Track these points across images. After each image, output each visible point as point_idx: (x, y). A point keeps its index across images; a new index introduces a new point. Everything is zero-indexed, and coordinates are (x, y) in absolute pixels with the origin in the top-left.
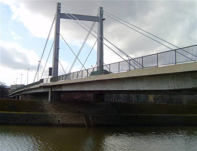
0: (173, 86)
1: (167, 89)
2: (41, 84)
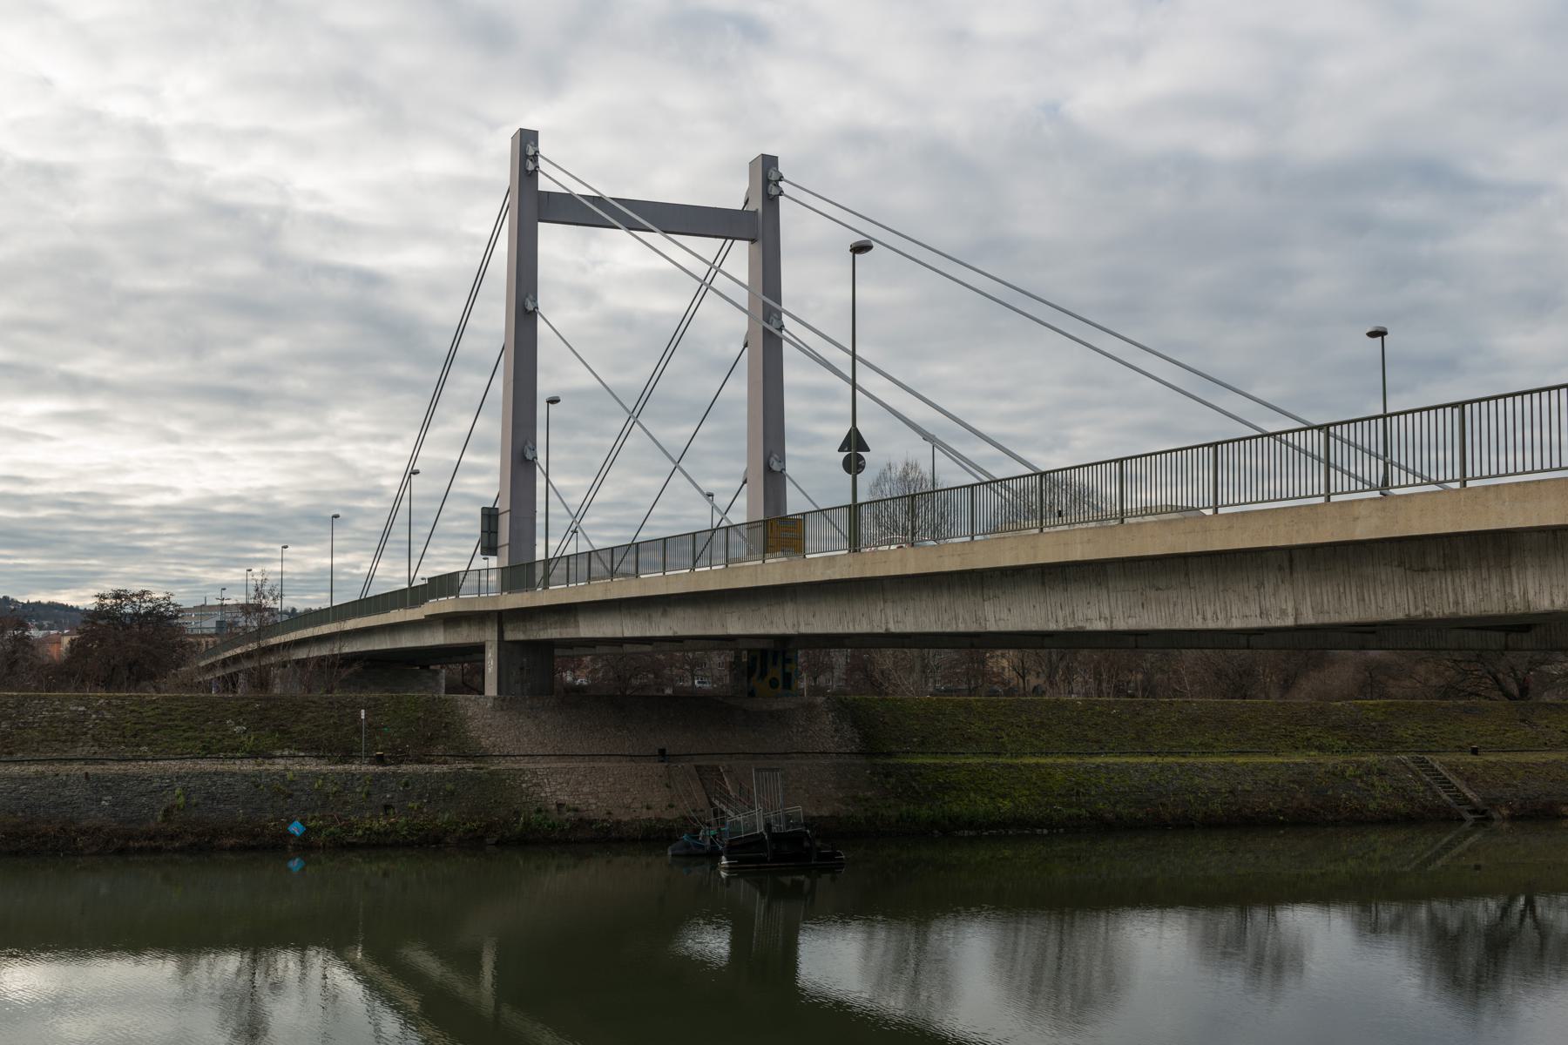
0: (1290, 610)
1: (1255, 622)
2: (444, 605)
